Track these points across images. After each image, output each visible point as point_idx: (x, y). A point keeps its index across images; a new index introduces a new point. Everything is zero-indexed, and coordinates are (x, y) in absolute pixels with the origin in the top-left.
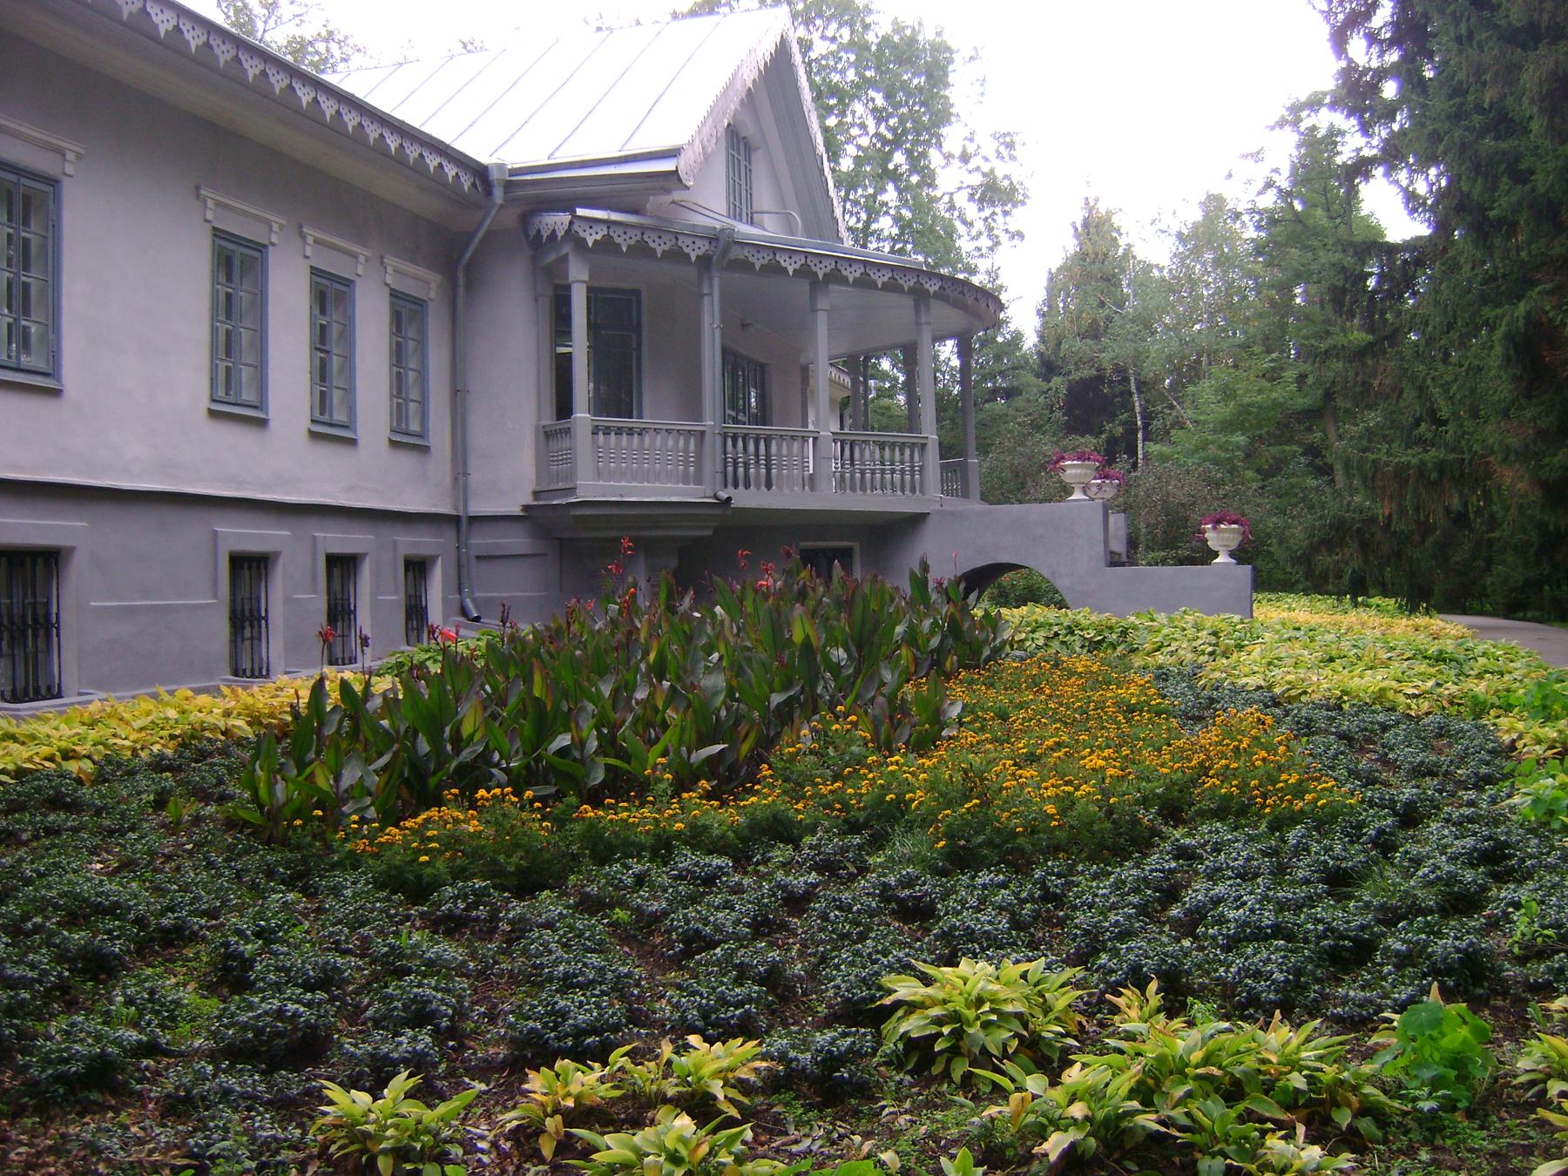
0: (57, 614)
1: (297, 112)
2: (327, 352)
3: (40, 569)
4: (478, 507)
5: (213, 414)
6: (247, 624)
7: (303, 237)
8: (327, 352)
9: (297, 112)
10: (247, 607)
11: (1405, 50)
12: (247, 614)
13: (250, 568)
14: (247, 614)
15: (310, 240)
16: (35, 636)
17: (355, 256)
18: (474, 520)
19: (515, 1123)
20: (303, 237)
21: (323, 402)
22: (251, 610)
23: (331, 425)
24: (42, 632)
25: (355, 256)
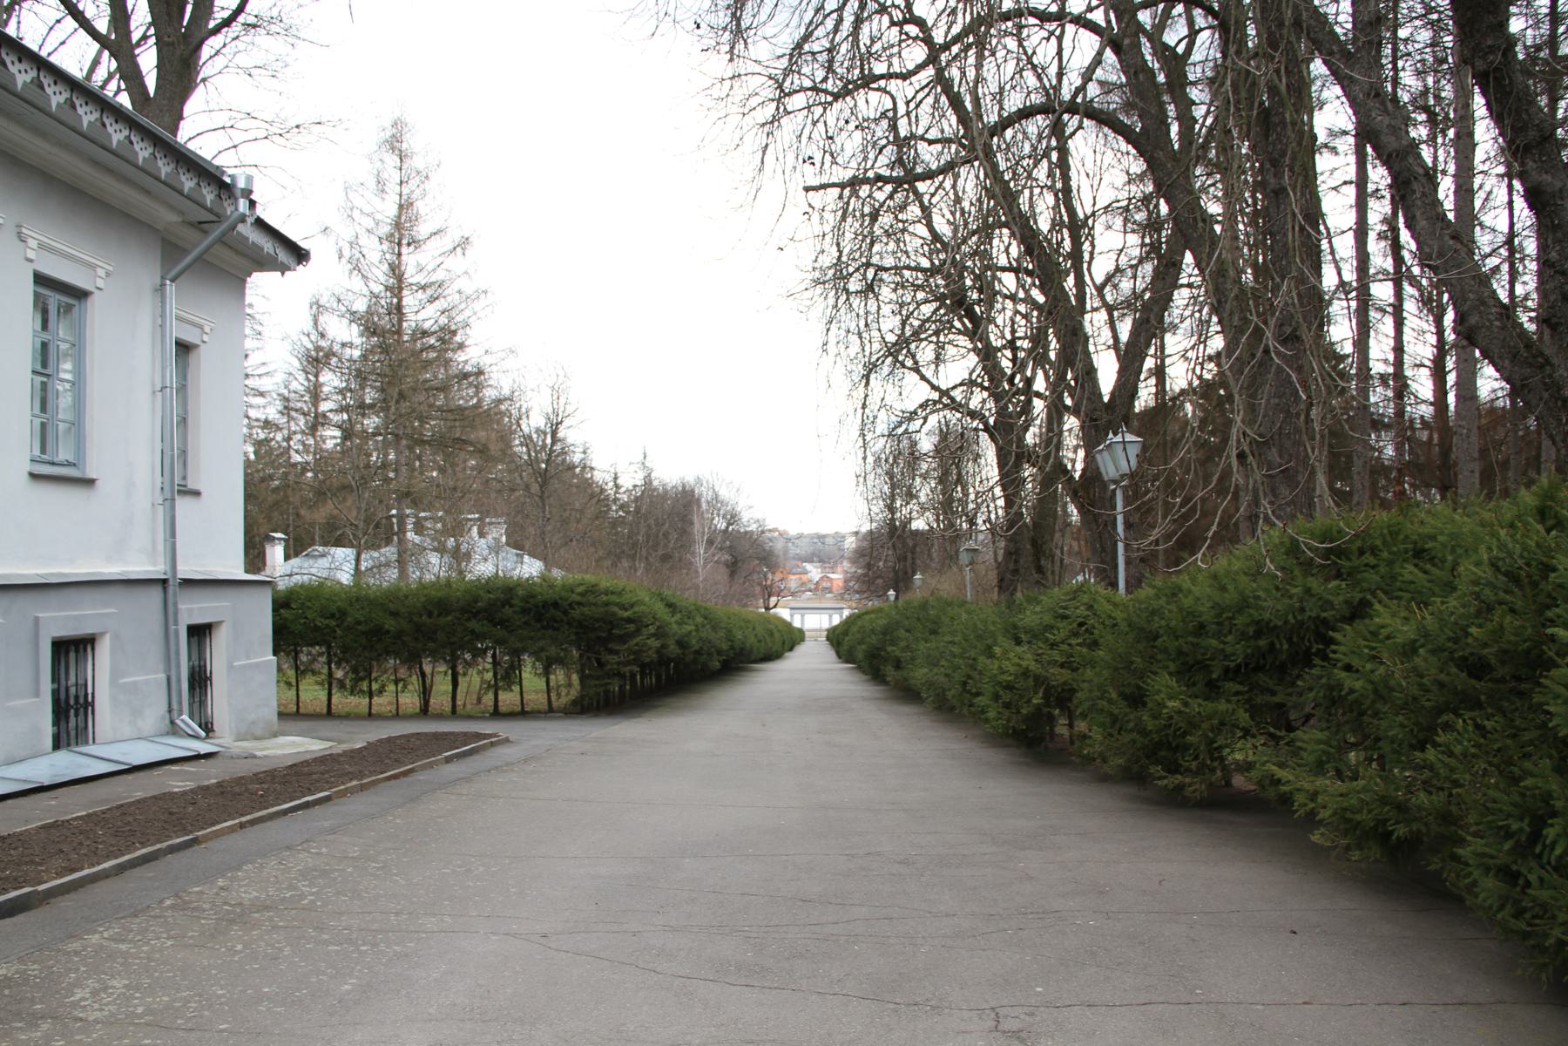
0: (93, 694)
1: (74, 130)
2: (48, 376)
3: (72, 655)
4: (186, 570)
5: (34, 476)
6: (72, 712)
7: (22, 238)
8: (48, 376)
9: (74, 130)
10: (73, 690)
11: (1177, 419)
12: (72, 702)
13: (77, 651)
14: (72, 702)
15: (33, 243)
16: (76, 715)
17: (93, 267)
18: (188, 583)
19: (1520, 204)
20: (22, 238)
21: (44, 435)
22: (77, 697)
23: (53, 464)
24: (82, 710)
25: (93, 267)
